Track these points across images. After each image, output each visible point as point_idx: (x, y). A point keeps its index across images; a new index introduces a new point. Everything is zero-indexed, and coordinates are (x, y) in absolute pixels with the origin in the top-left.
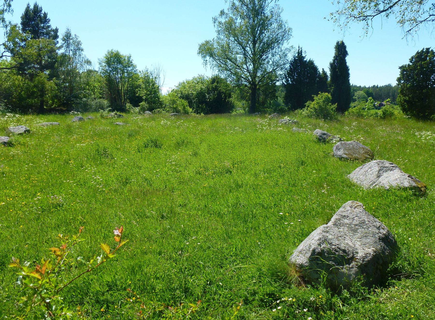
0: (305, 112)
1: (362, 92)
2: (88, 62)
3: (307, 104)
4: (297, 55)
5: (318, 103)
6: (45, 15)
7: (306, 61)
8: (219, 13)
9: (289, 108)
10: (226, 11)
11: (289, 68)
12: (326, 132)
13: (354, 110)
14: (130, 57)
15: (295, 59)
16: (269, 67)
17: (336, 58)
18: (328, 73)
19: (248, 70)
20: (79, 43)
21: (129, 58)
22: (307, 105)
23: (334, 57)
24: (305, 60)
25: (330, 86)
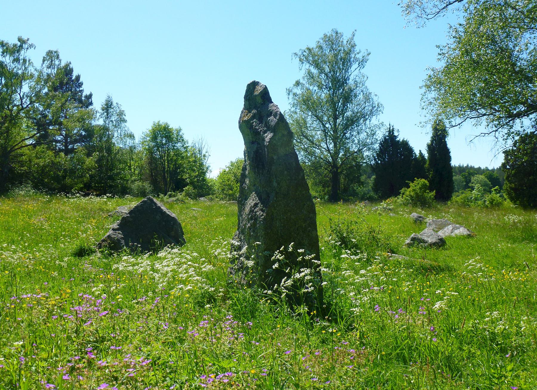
0: (400, 200)
1: (482, 177)
2: (131, 136)
3: (402, 191)
4: (387, 134)
5: (414, 190)
6: (78, 78)
7: (399, 141)
8: (294, 83)
9: (379, 197)
10: (301, 81)
11: (378, 148)
12: (422, 216)
13: (458, 199)
14: (180, 130)
15: (385, 138)
16: (354, 146)
17: (433, 139)
18: (426, 155)
19: (328, 150)
20: (121, 114)
21: (179, 131)
22: (402, 193)
23: (432, 137)
24: (397, 139)
25: (429, 171)
